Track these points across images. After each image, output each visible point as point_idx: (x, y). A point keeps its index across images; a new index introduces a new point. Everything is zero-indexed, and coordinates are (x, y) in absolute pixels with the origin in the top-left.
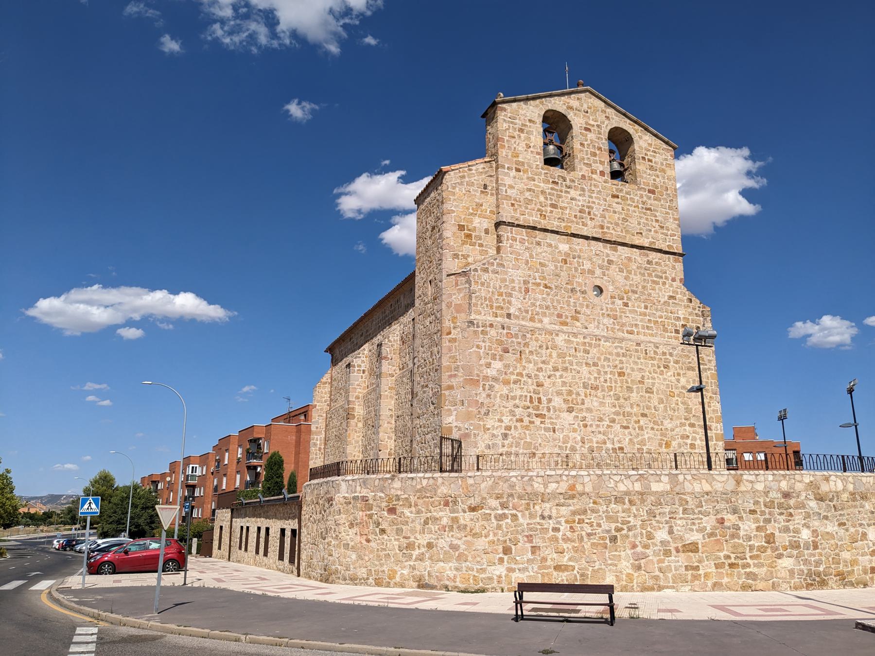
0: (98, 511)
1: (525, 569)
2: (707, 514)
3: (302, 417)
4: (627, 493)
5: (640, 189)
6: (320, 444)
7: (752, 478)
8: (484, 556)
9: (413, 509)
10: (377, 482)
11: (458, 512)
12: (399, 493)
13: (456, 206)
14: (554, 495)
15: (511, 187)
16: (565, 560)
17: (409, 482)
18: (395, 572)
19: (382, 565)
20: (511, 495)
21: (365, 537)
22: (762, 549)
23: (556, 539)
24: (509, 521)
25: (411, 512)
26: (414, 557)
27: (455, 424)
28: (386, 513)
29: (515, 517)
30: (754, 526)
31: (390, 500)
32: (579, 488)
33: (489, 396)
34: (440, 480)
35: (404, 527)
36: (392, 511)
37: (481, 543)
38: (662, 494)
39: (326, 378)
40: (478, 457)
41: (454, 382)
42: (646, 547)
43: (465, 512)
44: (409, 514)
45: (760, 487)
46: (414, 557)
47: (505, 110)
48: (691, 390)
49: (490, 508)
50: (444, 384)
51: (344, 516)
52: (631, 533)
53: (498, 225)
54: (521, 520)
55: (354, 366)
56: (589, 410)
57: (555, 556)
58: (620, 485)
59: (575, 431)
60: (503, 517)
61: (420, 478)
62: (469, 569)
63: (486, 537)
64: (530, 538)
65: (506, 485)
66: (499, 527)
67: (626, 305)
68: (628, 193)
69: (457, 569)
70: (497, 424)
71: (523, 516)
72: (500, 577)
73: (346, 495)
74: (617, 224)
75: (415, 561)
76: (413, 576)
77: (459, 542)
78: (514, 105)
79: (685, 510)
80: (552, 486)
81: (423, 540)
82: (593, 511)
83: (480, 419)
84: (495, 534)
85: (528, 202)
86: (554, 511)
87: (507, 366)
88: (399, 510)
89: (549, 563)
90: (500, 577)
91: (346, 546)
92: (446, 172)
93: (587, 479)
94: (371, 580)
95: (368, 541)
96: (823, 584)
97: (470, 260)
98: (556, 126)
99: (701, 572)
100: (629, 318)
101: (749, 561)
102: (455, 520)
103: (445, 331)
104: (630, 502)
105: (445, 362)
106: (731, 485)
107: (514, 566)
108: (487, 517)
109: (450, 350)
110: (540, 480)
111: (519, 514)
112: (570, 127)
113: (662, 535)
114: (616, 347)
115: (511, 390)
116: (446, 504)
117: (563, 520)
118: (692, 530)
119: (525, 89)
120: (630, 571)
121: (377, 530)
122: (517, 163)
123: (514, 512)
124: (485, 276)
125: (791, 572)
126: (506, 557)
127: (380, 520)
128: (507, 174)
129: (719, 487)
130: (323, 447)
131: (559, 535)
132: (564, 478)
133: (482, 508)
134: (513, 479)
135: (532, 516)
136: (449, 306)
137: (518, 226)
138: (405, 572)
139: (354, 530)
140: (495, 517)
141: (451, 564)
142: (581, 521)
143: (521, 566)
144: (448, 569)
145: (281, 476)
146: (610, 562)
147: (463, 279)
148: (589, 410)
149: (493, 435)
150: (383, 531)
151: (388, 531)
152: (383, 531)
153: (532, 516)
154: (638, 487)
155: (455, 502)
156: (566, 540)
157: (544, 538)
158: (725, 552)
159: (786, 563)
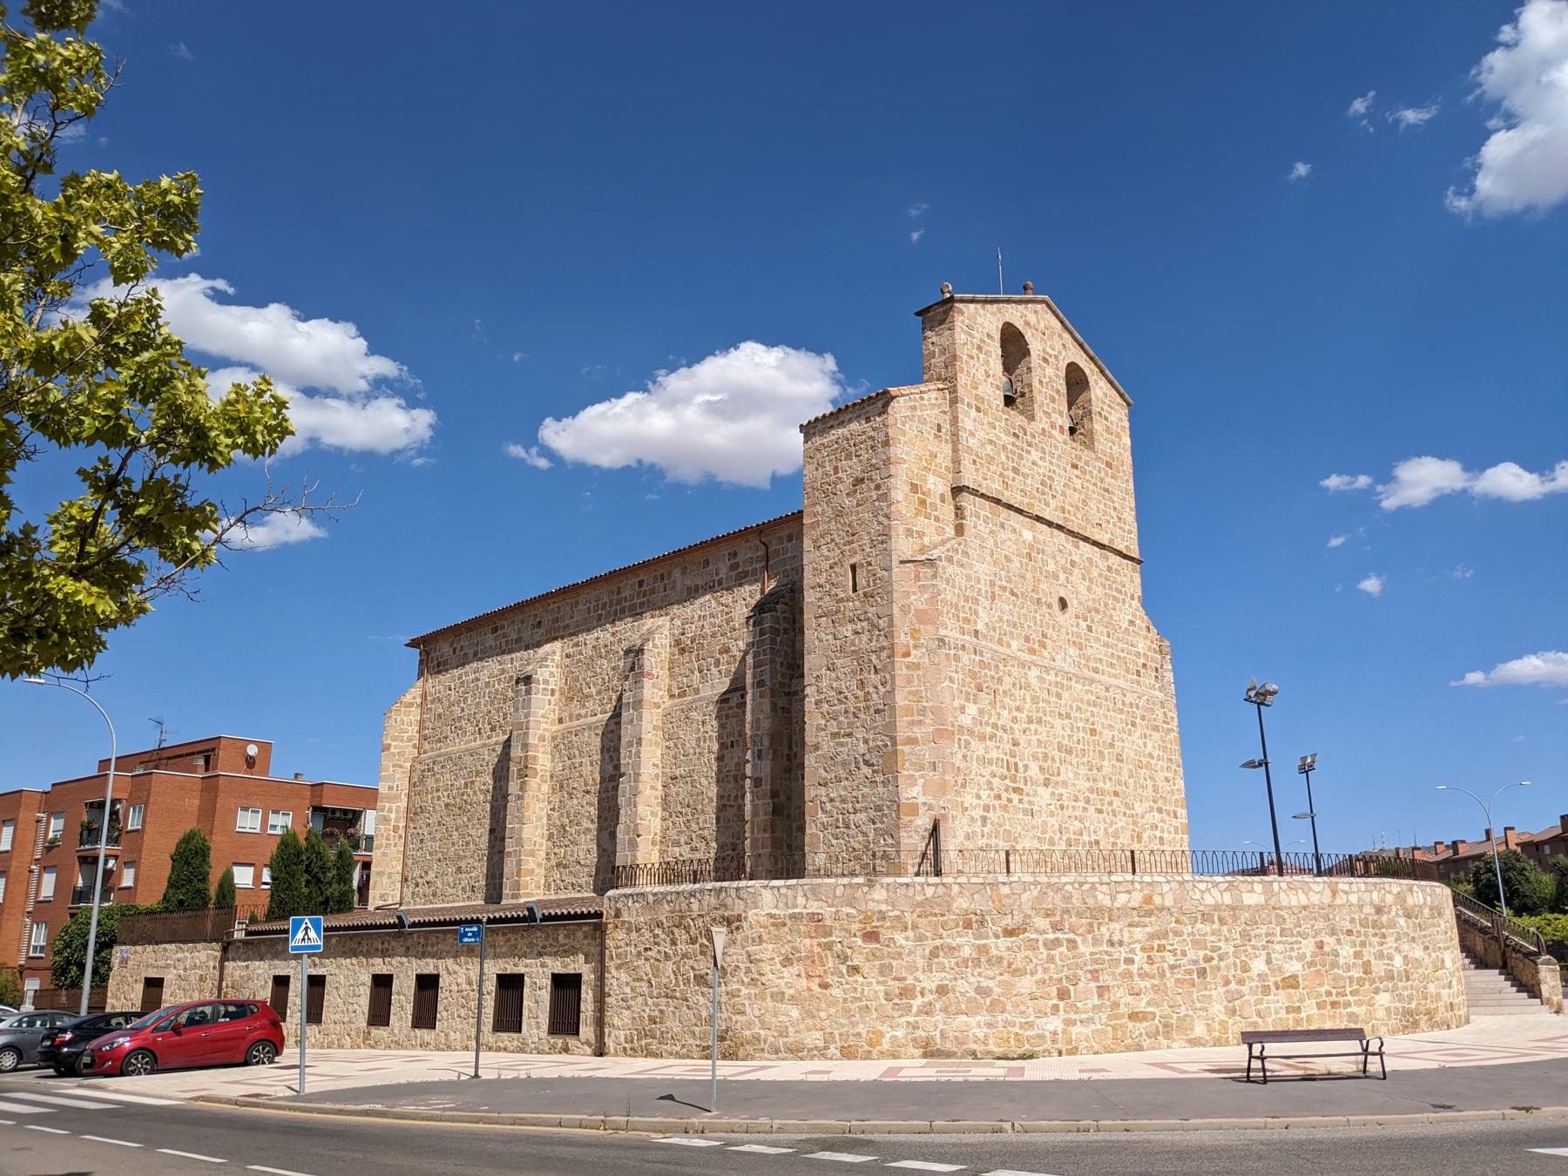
0: (321, 943)
1: (1091, 1020)
2: (1304, 936)
3: (201, 762)
4: (1216, 907)
5: (1098, 459)
6: (397, 820)
7: (1346, 887)
8: (1030, 1003)
9: (910, 933)
10: (839, 891)
11: (987, 937)
12: (883, 908)
13: (908, 454)
14: (1125, 910)
15: (972, 434)
16: (1142, 1005)
17: (902, 891)
18: (881, 1034)
19: (853, 1025)
20: (1067, 911)
21: (817, 980)
22: (1361, 982)
23: (1129, 975)
24: (1064, 949)
25: (907, 939)
26: (914, 1010)
27: (921, 799)
28: (859, 941)
29: (1072, 944)
30: (1351, 951)
31: (867, 919)
32: (1157, 900)
33: (965, 757)
34: (956, 889)
35: (894, 963)
36: (871, 936)
37: (1026, 984)
38: (1259, 908)
39: (413, 694)
40: (1007, 854)
41: (918, 732)
42: (1241, 982)
43: (997, 937)
44: (903, 942)
45: (1354, 899)
46: (914, 1010)
47: (962, 313)
48: (1251, 765)
49: (1037, 931)
50: (901, 735)
51: (770, 947)
52: (1222, 964)
53: (957, 491)
54: (1082, 948)
55: (538, 682)
56: (1065, 784)
57: (1129, 999)
58: (1207, 896)
59: (1052, 814)
60: (1057, 943)
61: (922, 885)
62: (1007, 1023)
63: (1032, 974)
64: (1095, 975)
65: (1058, 897)
66: (1051, 959)
67: (1090, 629)
68: (1087, 463)
69: (989, 1025)
70: (975, 802)
71: (1084, 941)
72: (1055, 1033)
73: (774, 911)
74: (1077, 508)
75: (917, 1015)
76: (915, 1040)
77: (991, 984)
78: (972, 306)
79: (1283, 930)
80: (1122, 898)
81: (930, 982)
82: (1176, 933)
83: (958, 793)
84: (1045, 970)
85: (991, 460)
86: (1126, 934)
87: (981, 712)
88: (885, 935)
89: (1123, 1009)
90: (1055, 1033)
91: (779, 996)
92: (893, 398)
93: (1166, 888)
94: (833, 1050)
95: (825, 986)
96: (1415, 1026)
97: (926, 540)
98: (1013, 345)
99: (1303, 1015)
100: (1096, 650)
101: (1349, 998)
102: (983, 949)
103: (899, 650)
104: (1221, 920)
105: (901, 700)
106: (1327, 899)
107: (1073, 1016)
108: (1032, 945)
109: (909, 682)
110: (1105, 888)
111: (1079, 940)
112: (1027, 353)
113: (1259, 966)
114: (1087, 692)
115: (987, 750)
116: (968, 925)
117: (1137, 946)
118: (1291, 958)
119: (988, 290)
120: (1224, 1018)
121: (843, 969)
122: (978, 398)
123: (1072, 936)
124: (950, 569)
125: (1388, 1010)
126: (1062, 1004)
127: (849, 952)
128: (967, 414)
129: (1315, 899)
130: (402, 824)
131: (1134, 968)
132: (1137, 886)
133: (1025, 930)
134: (1068, 888)
135: (1096, 942)
136: (905, 610)
137: (982, 496)
138: (899, 1033)
139: (794, 970)
140: (1045, 945)
141: (979, 1018)
142: (1161, 949)
143: (1084, 1016)
144: (974, 1025)
145: (204, 878)
146: (1198, 1005)
147: (926, 571)
148: (1065, 784)
149: (972, 819)
150: (855, 970)
151: (865, 970)
152: (855, 970)
153: (1096, 942)
154: (1227, 899)
155: (982, 923)
156: (1144, 975)
157: (1113, 974)
158: (1326, 987)
159: (1384, 999)
